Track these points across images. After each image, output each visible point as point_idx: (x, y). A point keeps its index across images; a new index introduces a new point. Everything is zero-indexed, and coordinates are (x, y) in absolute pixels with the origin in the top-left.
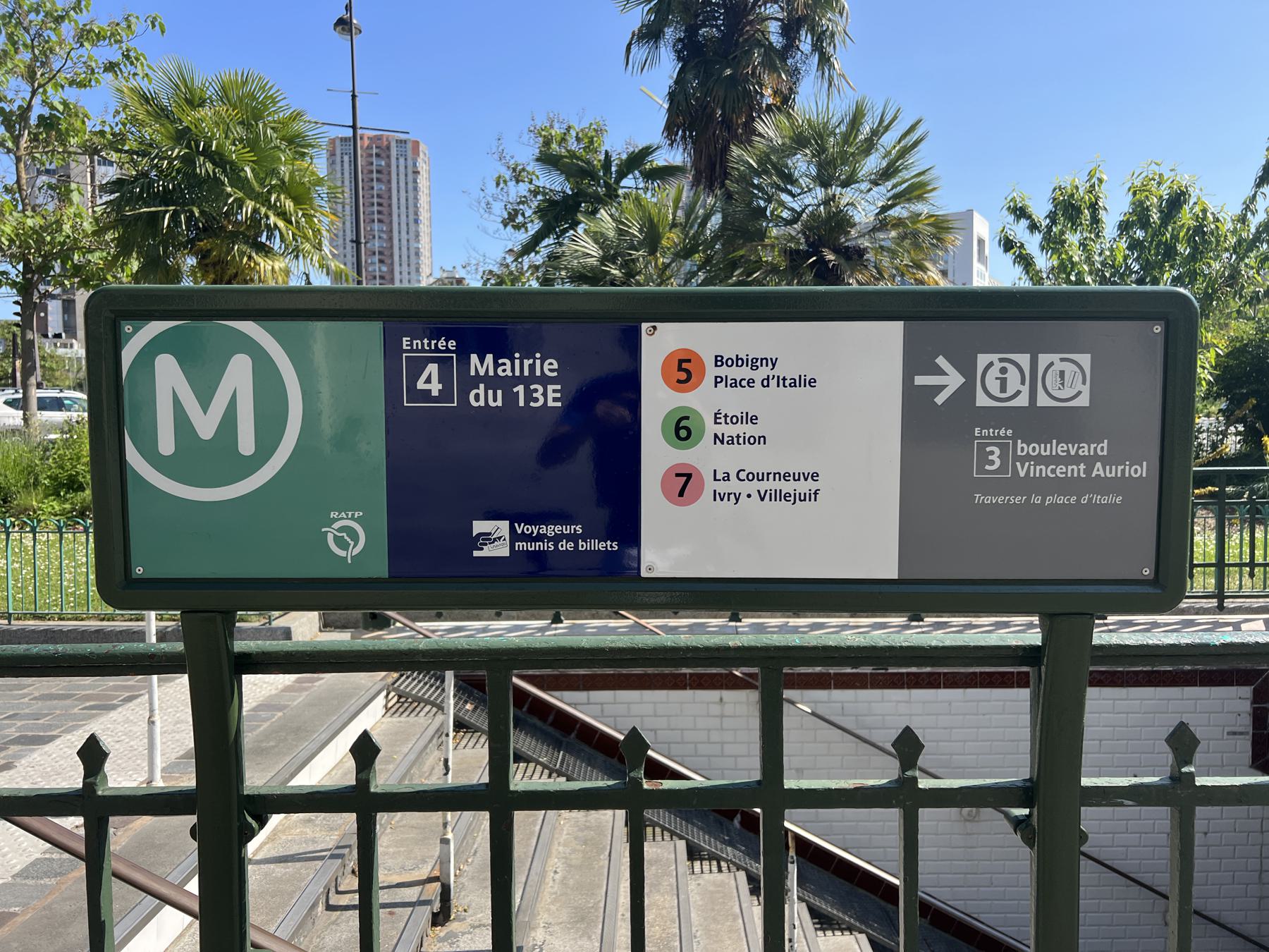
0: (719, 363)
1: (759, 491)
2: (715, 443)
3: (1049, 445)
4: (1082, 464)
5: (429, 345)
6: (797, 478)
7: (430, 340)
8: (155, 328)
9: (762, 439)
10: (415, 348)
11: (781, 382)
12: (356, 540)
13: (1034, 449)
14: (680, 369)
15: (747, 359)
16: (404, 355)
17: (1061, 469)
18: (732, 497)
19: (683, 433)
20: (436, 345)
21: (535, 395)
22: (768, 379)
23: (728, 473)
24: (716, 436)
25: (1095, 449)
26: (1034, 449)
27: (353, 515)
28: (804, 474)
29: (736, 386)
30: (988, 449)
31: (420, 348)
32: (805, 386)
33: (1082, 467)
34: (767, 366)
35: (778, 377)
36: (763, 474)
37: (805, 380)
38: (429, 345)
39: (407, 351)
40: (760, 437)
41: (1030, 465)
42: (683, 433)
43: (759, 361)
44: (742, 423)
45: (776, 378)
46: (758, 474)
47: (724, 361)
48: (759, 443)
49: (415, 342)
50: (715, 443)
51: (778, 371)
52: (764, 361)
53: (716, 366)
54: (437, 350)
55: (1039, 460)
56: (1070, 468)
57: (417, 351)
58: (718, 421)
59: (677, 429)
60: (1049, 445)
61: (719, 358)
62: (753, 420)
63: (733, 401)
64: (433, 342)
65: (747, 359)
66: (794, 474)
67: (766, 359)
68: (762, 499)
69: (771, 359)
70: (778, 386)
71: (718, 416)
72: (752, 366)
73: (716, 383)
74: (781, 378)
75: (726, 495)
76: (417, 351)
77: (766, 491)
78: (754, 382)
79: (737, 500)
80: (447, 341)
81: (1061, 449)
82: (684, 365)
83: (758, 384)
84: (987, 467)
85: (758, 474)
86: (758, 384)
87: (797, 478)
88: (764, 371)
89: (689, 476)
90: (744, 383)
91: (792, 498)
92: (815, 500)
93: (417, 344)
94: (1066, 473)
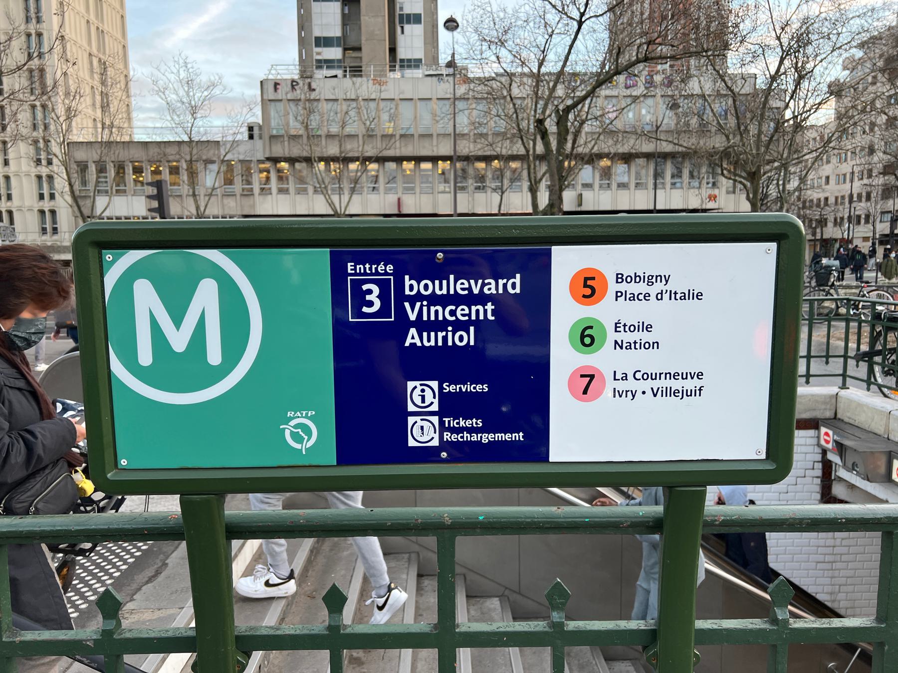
0: (620, 280)
1: (652, 389)
2: (615, 349)
3: (445, 282)
4: (489, 304)
5: (370, 269)
6: (684, 377)
7: (371, 265)
8: (134, 256)
9: (656, 344)
10: (358, 271)
11: (673, 296)
12: (309, 434)
13: (426, 287)
14: (585, 286)
15: (644, 276)
16: (349, 278)
17: (463, 310)
18: (629, 394)
19: (587, 340)
20: (376, 269)
21: (368, 297)
22: (662, 293)
23: (626, 374)
24: (616, 342)
25: (505, 285)
26: (426, 287)
27: (307, 414)
28: (690, 373)
29: (634, 300)
30: (365, 287)
31: (362, 271)
32: (693, 299)
33: (490, 307)
34: (661, 282)
35: (671, 291)
36: (656, 374)
37: (693, 293)
38: (370, 269)
39: (351, 275)
40: (654, 343)
41: (422, 306)
42: (587, 340)
43: (654, 278)
44: (638, 331)
45: (668, 292)
46: (652, 374)
47: (624, 278)
48: (653, 348)
49: (358, 267)
50: (615, 349)
51: (671, 286)
52: (659, 278)
53: (617, 282)
54: (377, 273)
55: (434, 300)
56: (474, 308)
57: (360, 274)
58: (618, 329)
59: (583, 336)
60: (445, 282)
61: (620, 276)
62: (649, 328)
63: (631, 312)
64: (374, 267)
65: (644, 276)
66: (682, 373)
67: (661, 276)
68: (655, 395)
69: (665, 276)
70: (670, 299)
71: (618, 325)
72: (648, 282)
73: (617, 297)
74: (673, 292)
75: (624, 393)
76: (360, 274)
77: (659, 388)
78: (649, 296)
79: (634, 396)
80: (385, 266)
81: (460, 287)
82: (589, 283)
83: (653, 297)
84: (365, 309)
85: (652, 374)
86: (653, 297)
87: (684, 377)
88: (658, 287)
89: (592, 377)
90: (641, 297)
91: (680, 394)
92: (700, 395)
93: (360, 268)
94: (469, 315)
